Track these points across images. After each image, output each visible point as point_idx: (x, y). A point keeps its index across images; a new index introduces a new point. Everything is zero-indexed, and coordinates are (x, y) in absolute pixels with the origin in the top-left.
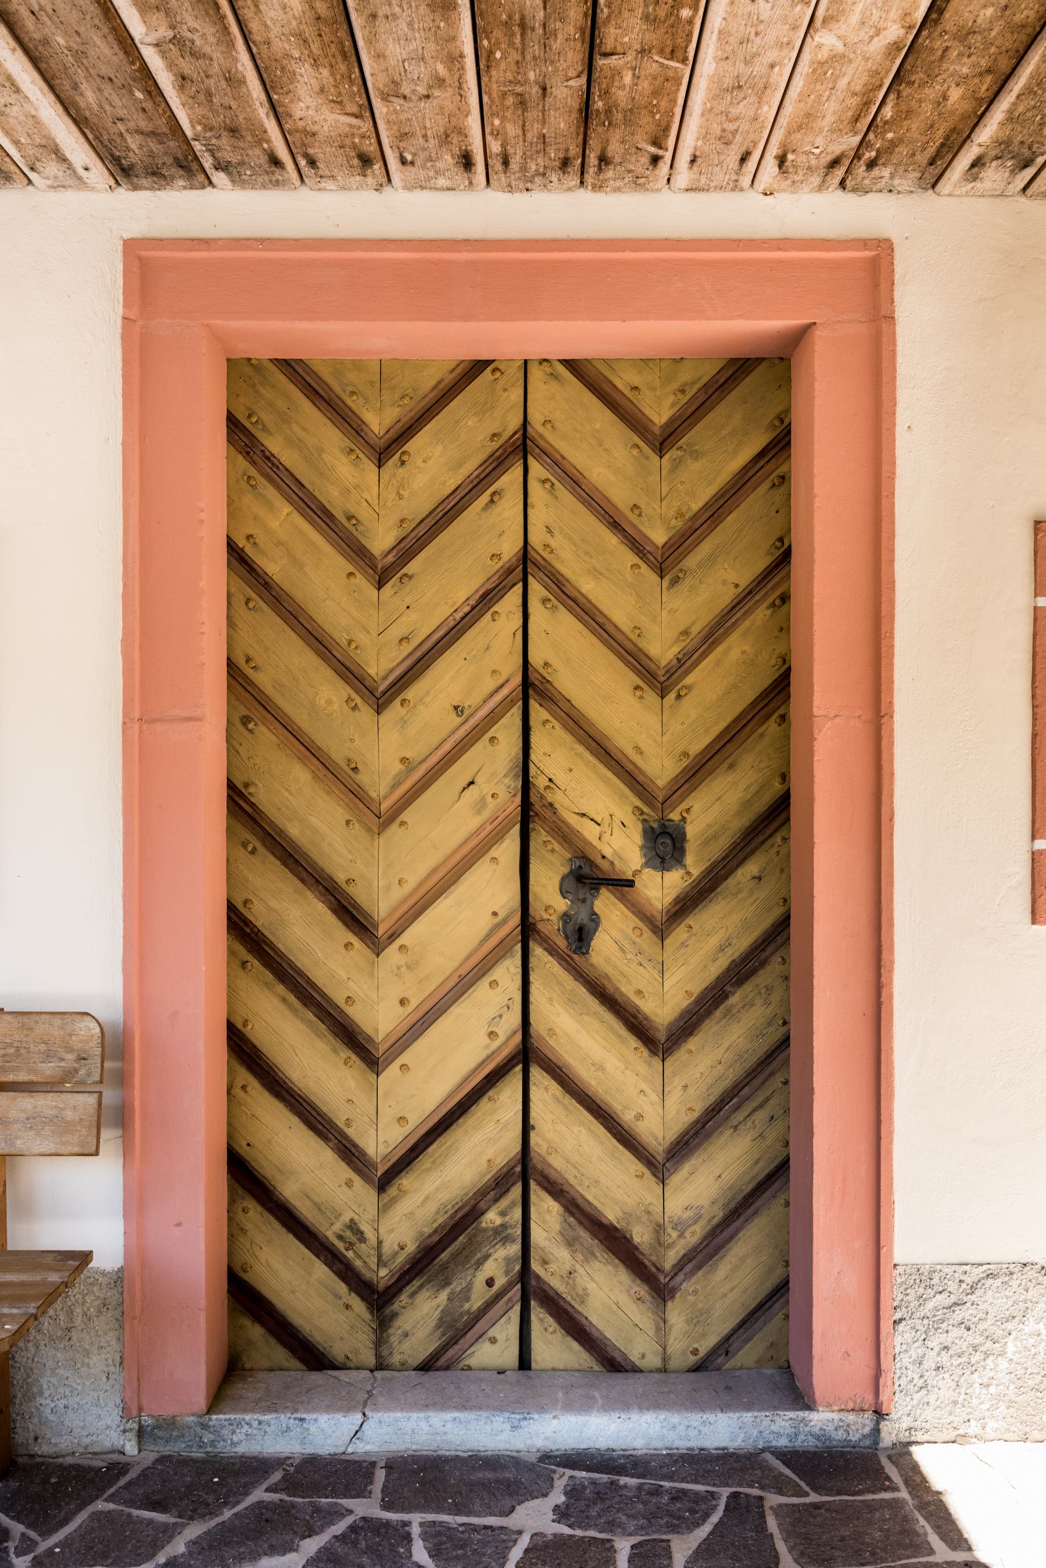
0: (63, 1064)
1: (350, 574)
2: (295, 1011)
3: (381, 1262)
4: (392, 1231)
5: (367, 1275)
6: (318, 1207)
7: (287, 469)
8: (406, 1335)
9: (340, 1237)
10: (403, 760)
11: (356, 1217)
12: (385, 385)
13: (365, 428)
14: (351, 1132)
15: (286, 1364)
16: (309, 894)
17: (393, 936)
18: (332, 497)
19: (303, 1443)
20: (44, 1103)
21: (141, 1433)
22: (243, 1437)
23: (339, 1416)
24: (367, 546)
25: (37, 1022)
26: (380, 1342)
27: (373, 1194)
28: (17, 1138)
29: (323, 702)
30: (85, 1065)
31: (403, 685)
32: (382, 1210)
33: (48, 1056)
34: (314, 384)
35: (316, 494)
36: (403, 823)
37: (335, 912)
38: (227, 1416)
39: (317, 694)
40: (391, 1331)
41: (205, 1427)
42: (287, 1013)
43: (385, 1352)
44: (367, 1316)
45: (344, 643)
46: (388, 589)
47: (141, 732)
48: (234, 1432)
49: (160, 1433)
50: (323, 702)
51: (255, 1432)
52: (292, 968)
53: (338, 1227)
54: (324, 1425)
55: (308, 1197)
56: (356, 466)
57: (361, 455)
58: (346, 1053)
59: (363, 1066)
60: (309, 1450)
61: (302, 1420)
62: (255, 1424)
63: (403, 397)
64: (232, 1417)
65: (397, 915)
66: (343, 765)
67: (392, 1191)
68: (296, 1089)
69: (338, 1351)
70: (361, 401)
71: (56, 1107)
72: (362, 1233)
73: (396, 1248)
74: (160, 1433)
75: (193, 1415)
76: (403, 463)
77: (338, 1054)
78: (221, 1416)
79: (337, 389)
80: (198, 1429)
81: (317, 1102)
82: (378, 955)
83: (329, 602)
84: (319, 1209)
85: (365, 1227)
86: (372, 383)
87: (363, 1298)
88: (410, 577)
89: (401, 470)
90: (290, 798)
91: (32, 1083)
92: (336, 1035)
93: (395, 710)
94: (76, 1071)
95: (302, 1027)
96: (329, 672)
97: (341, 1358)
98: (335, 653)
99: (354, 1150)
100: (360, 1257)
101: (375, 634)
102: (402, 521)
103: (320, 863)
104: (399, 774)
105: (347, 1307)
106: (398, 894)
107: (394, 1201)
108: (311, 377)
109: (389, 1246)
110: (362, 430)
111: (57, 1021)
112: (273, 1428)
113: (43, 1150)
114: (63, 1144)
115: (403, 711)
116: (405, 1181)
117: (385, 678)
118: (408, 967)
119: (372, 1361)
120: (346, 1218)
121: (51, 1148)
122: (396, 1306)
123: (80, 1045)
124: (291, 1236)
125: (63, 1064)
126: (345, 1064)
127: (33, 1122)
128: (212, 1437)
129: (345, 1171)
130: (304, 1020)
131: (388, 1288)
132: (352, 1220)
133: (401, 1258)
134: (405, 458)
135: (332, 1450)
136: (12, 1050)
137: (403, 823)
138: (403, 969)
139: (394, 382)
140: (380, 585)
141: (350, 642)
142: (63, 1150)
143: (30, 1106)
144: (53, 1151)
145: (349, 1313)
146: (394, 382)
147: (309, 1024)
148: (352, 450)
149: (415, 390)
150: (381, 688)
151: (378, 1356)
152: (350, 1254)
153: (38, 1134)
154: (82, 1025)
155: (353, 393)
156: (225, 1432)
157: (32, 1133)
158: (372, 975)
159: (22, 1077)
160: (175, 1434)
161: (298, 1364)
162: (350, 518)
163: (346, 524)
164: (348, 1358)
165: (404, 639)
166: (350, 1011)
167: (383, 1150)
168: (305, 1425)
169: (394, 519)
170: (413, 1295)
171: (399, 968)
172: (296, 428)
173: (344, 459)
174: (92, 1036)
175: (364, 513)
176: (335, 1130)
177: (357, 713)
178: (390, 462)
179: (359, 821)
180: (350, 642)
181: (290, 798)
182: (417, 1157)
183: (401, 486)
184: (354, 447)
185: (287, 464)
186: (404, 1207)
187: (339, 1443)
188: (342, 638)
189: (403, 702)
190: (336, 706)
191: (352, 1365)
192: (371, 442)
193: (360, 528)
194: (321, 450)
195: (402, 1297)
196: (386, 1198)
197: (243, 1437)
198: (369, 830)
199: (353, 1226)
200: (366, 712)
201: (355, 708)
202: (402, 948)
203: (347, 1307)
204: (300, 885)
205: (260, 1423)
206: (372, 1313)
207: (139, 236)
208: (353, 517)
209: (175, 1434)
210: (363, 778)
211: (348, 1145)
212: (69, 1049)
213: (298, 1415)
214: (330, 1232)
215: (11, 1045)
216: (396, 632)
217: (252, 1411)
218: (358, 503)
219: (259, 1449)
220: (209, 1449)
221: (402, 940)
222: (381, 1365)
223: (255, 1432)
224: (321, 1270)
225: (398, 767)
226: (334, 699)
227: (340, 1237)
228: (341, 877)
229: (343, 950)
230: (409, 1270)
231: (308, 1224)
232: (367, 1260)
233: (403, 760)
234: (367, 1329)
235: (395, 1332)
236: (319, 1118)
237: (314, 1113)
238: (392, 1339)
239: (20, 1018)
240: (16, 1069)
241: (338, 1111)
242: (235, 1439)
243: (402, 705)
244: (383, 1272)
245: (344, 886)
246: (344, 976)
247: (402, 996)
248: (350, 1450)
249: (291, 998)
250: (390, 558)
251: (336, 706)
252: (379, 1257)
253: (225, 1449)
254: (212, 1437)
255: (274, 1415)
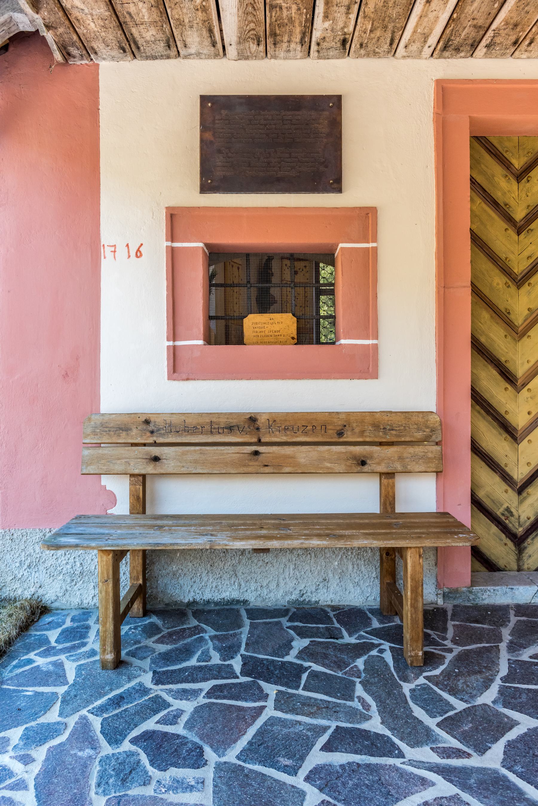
0: (425, 433)
1: (506, 230)
2: (484, 418)
3: (520, 525)
4: (524, 511)
5: (514, 530)
6: (493, 501)
7: (479, 184)
8: (530, 556)
9: (503, 514)
10: (529, 309)
11: (509, 506)
12: (520, 148)
13: (512, 166)
14: (507, 469)
15: (480, 569)
16: (490, 367)
17: (524, 385)
18: (498, 196)
19: (512, 599)
20: (418, 450)
21: (445, 596)
22: (487, 596)
23: (528, 587)
24: (513, 217)
25: (412, 416)
26: (519, 559)
27: (516, 495)
28: (408, 465)
29: (495, 284)
30: (435, 434)
31: (527, 278)
32: (521, 502)
33: (419, 429)
34: (489, 148)
35: (492, 195)
36: (529, 336)
37: (500, 374)
38: (480, 588)
39: (493, 281)
40: (524, 555)
41: (470, 592)
42: (480, 418)
43: (521, 564)
44: (514, 548)
45: (503, 259)
46: (522, 236)
47: (465, 287)
48: (483, 595)
49: (451, 595)
50: (495, 284)
51: (492, 594)
52: (482, 399)
53: (502, 510)
54: (522, 591)
55: (489, 497)
56: (508, 182)
57: (511, 178)
58: (505, 435)
59: (512, 440)
60: (515, 602)
61: (512, 589)
62: (492, 591)
63: (528, 153)
64: (482, 588)
65: (525, 376)
66: (503, 311)
67: (524, 494)
68: (484, 451)
69: (501, 563)
70: (511, 154)
71: (424, 452)
72: (512, 512)
73: (526, 519)
74: (451, 595)
75: (465, 587)
76: (528, 181)
77: (502, 435)
78: (477, 588)
79: (500, 149)
80: (468, 593)
81: (493, 456)
82: (518, 393)
83: (497, 241)
84: (494, 502)
85: (513, 510)
86: (515, 147)
87: (512, 541)
88: (532, 230)
89: (527, 184)
90: (482, 326)
91: (412, 442)
92: (501, 427)
93: (526, 287)
94: (431, 436)
95: (487, 424)
96: (497, 271)
97: (503, 567)
98: (499, 263)
99: (507, 477)
100: (511, 523)
101: (517, 255)
102: (528, 206)
103: (494, 353)
104: (527, 315)
105: (506, 544)
106: (527, 366)
107: (525, 498)
108: (488, 144)
109: (523, 518)
110: (510, 167)
111: (421, 415)
112: (500, 592)
113: (420, 470)
114: (429, 467)
115: (529, 288)
116: (530, 490)
117: (521, 274)
118: (531, 398)
119: (516, 567)
120: (505, 506)
121: (423, 469)
122: (526, 544)
123: (431, 425)
124: (481, 514)
125: (425, 433)
126: (505, 440)
127: (415, 458)
128: (474, 597)
129: (505, 486)
130: (487, 421)
131: (521, 536)
132: (507, 507)
133: (528, 523)
134: (529, 179)
135: (525, 602)
136: (402, 428)
137: (529, 336)
138: (529, 399)
139: (524, 146)
140: (519, 234)
141: (506, 259)
142: (428, 470)
143: (412, 451)
144: (424, 470)
145: (506, 547)
146: (524, 146)
147: (489, 423)
148: (507, 176)
149: (533, 150)
150: (519, 278)
151: (519, 566)
152: (507, 522)
153: (417, 463)
154: (432, 417)
155: (507, 151)
156: (479, 595)
157: (414, 463)
158: (516, 402)
159: (408, 439)
160: (458, 596)
161: (485, 569)
162: (506, 205)
163: (505, 208)
164: (506, 566)
165: (529, 257)
166: (507, 417)
167: (521, 477)
168: (513, 591)
169: (524, 205)
170: (533, 539)
171: (527, 398)
172: (482, 166)
173: (503, 179)
174: (437, 421)
175: (512, 203)
176: (500, 468)
177: (509, 289)
178: (523, 181)
179: (510, 335)
180: (506, 259)
181: (482, 326)
182: (534, 480)
183: (528, 191)
184: (507, 174)
185: (479, 181)
186: (530, 501)
187: (528, 598)
188: (503, 256)
189: (529, 284)
190: (501, 286)
191: (507, 569)
192: (514, 172)
193: (511, 209)
194: (493, 176)
195: (529, 540)
196: (521, 497)
197: (487, 596)
198: (515, 339)
199: (508, 510)
200: (513, 288)
201: (509, 287)
202: (529, 390)
203: (506, 544)
204: (486, 363)
205: (494, 590)
206: (516, 547)
207: (440, 78)
208: (507, 204)
209: (458, 596)
210: (512, 317)
211: (505, 475)
212: (427, 427)
213: (510, 587)
214: (499, 512)
215: (402, 425)
216: (526, 254)
217: (490, 585)
218: (510, 198)
219: (494, 601)
220: (472, 602)
221: (529, 386)
222: (519, 570)
223: (492, 594)
224: (494, 529)
225: (527, 312)
226: (500, 282)
227: (503, 514)
228: (503, 359)
229: (504, 391)
230: (530, 528)
231: (489, 509)
232: (514, 524)
233: (529, 309)
234: (513, 554)
235: (525, 555)
236: (492, 463)
237: (490, 461)
238: (524, 558)
239: (404, 414)
240: (405, 436)
241: (502, 461)
242: (483, 597)
243: (529, 285)
244: (521, 529)
245: (504, 363)
246: (505, 402)
247: (529, 410)
248: (533, 602)
249: (482, 412)
250: (522, 223)
251: (501, 286)
252: (519, 523)
253: (480, 602)
254: (474, 597)
255: (500, 587)
